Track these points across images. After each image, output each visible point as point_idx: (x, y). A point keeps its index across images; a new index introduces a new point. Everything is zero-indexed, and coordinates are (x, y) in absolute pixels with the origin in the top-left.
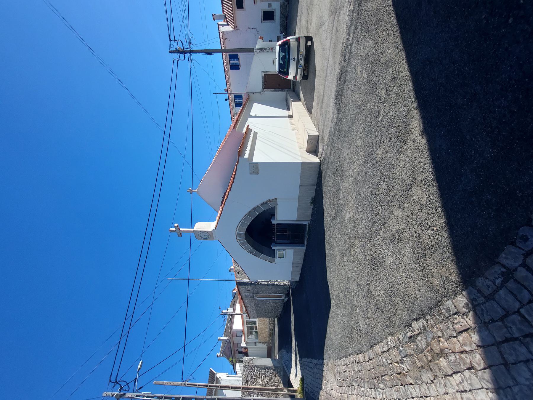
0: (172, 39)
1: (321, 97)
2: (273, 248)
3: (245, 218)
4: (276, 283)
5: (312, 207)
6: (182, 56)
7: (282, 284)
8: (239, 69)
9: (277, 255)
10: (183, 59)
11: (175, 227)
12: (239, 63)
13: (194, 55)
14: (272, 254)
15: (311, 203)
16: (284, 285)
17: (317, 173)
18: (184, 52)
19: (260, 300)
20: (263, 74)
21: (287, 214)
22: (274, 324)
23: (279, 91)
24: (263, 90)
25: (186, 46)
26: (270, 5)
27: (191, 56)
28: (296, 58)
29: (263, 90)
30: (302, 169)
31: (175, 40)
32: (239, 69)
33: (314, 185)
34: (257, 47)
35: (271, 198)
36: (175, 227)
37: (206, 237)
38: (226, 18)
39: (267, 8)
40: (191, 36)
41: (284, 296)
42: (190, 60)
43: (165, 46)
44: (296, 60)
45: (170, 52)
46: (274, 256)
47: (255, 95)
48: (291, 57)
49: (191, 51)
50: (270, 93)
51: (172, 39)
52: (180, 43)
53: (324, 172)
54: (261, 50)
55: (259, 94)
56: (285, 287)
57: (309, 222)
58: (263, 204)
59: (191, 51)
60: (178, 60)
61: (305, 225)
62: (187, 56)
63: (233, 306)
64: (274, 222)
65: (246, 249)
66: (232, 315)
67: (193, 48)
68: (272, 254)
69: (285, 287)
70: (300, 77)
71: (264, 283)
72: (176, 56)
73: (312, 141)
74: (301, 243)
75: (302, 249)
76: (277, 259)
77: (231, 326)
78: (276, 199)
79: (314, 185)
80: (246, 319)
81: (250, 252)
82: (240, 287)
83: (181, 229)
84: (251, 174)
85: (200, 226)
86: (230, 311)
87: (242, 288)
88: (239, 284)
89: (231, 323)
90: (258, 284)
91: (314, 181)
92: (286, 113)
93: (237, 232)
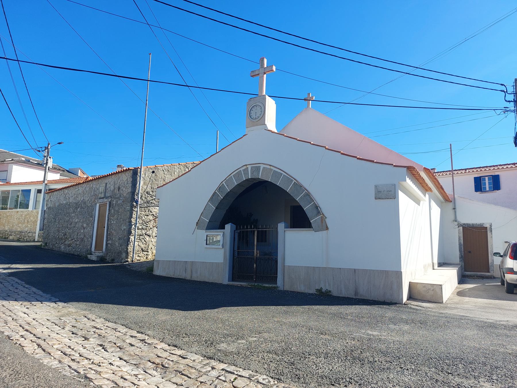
1: (508, 308)
2: (228, 227)
3: (289, 179)
4: (132, 238)
5: (311, 292)
7: (130, 248)
8: (476, 190)
9: (211, 233)
10: (507, 99)
11: (270, 66)
12: (486, 191)
14: (216, 223)
15: (320, 291)
16: (127, 253)
17: (381, 299)
19: (94, 209)
20: (488, 226)
21: (296, 248)
22: (18, 241)
23: (460, 251)
24: (459, 225)
27: (512, 111)
29: (459, 225)
30: (387, 272)
32: (476, 190)
33: (356, 293)
36: (270, 66)
37: (253, 116)
41: (99, 254)
42: (506, 110)
46: (211, 226)
47: (452, 212)
50: (456, 235)
53: (393, 307)
55: (453, 218)
56: (124, 255)
57: (281, 288)
58: (317, 207)
60: (506, 92)
61: (274, 279)
63: (55, 169)
65: (228, 180)
66: (40, 165)
68: (216, 223)
69: (124, 255)
70: (512, 280)
71: (134, 216)
73: (431, 293)
74: (234, 277)
76: (203, 234)
77: (19, 162)
78: (327, 228)
79: (356, 293)
80: (33, 189)
81: (221, 188)
82: (130, 173)
83: (265, 75)
84: (376, 186)
85: (271, 106)
86: (50, 164)
87: (127, 178)
88: (135, 173)
89: (24, 162)
90: (132, 206)
91: (364, 293)
92: (436, 261)
93: (262, 166)
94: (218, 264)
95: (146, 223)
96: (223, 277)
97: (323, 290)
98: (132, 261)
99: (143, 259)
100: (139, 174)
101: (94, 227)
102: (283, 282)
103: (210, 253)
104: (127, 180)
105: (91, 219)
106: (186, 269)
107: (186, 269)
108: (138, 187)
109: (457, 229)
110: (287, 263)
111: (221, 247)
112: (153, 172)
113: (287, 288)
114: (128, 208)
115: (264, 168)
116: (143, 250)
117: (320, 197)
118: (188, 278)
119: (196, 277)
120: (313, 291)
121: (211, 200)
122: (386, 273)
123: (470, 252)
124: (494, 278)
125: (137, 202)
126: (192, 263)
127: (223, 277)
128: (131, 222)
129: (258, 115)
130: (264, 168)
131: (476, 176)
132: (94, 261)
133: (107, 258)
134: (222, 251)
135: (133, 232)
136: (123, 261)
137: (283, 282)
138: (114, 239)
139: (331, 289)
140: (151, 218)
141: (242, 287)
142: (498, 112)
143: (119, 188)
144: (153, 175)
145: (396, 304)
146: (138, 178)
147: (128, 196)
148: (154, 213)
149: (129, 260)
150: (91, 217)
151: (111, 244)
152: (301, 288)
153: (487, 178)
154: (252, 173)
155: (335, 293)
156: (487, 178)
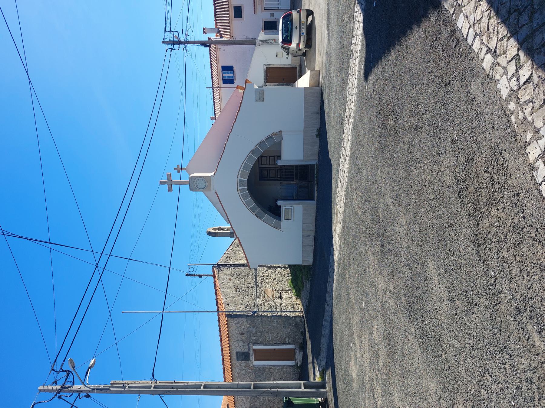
0: (168, 29)
3: (249, 158)
4: (284, 314)
6: (176, 47)
7: (292, 315)
8: (233, 83)
13: (189, 47)
15: (317, 136)
16: (296, 317)
17: (320, 99)
18: (179, 43)
20: (266, 67)
21: (293, 153)
24: (265, 85)
25: (182, 37)
26: (272, 15)
28: (298, 26)
29: (265, 85)
30: (305, 96)
31: (171, 31)
33: (317, 113)
34: (259, 38)
35: (276, 131)
37: (204, 185)
38: (220, 31)
39: (268, 18)
40: (188, 27)
43: (161, 35)
44: (298, 28)
45: (163, 42)
48: (294, 26)
49: (187, 43)
51: (168, 29)
52: (176, 34)
54: (263, 41)
57: (317, 161)
59: (187, 43)
61: (313, 166)
62: (182, 47)
64: (279, 163)
65: (247, 204)
67: (189, 39)
70: (303, 45)
72: (170, 46)
73: (314, 76)
74: (311, 198)
75: (313, 203)
78: (281, 131)
79: (317, 113)
81: (253, 210)
84: (256, 101)
88: (230, 316)
91: (317, 109)
93: (239, 178)
94: (304, 210)
95: (270, 307)
96: (312, 204)
97: (317, 133)
98: (302, 312)
99: (301, 306)
100: (231, 313)
101: (274, 365)
102: (313, 161)
103: (297, 214)
104: (235, 324)
105: (267, 370)
106: (308, 236)
107: (308, 236)
108: (242, 313)
109: (269, 87)
110: (302, 158)
111: (292, 208)
112: (228, 305)
113: (316, 157)
114: (259, 320)
115: (240, 177)
116: (293, 307)
117: (261, 137)
118: (313, 233)
119: (313, 227)
120: (317, 140)
121: (260, 218)
122: (305, 96)
123: (284, 79)
124: (301, 64)
125: (254, 313)
126: (304, 231)
127: (312, 204)
128: (271, 316)
129: (203, 182)
130: (240, 177)
131: (222, 82)
132: (303, 355)
133: (300, 341)
134: (295, 206)
135: (279, 314)
136: (303, 320)
137: (313, 161)
138: (284, 335)
139: (316, 128)
140: (266, 304)
141: (317, 190)
142: (186, 54)
143: (242, 334)
144: (230, 304)
145: (322, 91)
146: (235, 313)
147: (249, 322)
148: (263, 302)
149: (301, 315)
150: (264, 370)
151: (289, 338)
152: (316, 148)
153: (224, 75)
154: (244, 186)
155: (318, 126)
156: (224, 75)
